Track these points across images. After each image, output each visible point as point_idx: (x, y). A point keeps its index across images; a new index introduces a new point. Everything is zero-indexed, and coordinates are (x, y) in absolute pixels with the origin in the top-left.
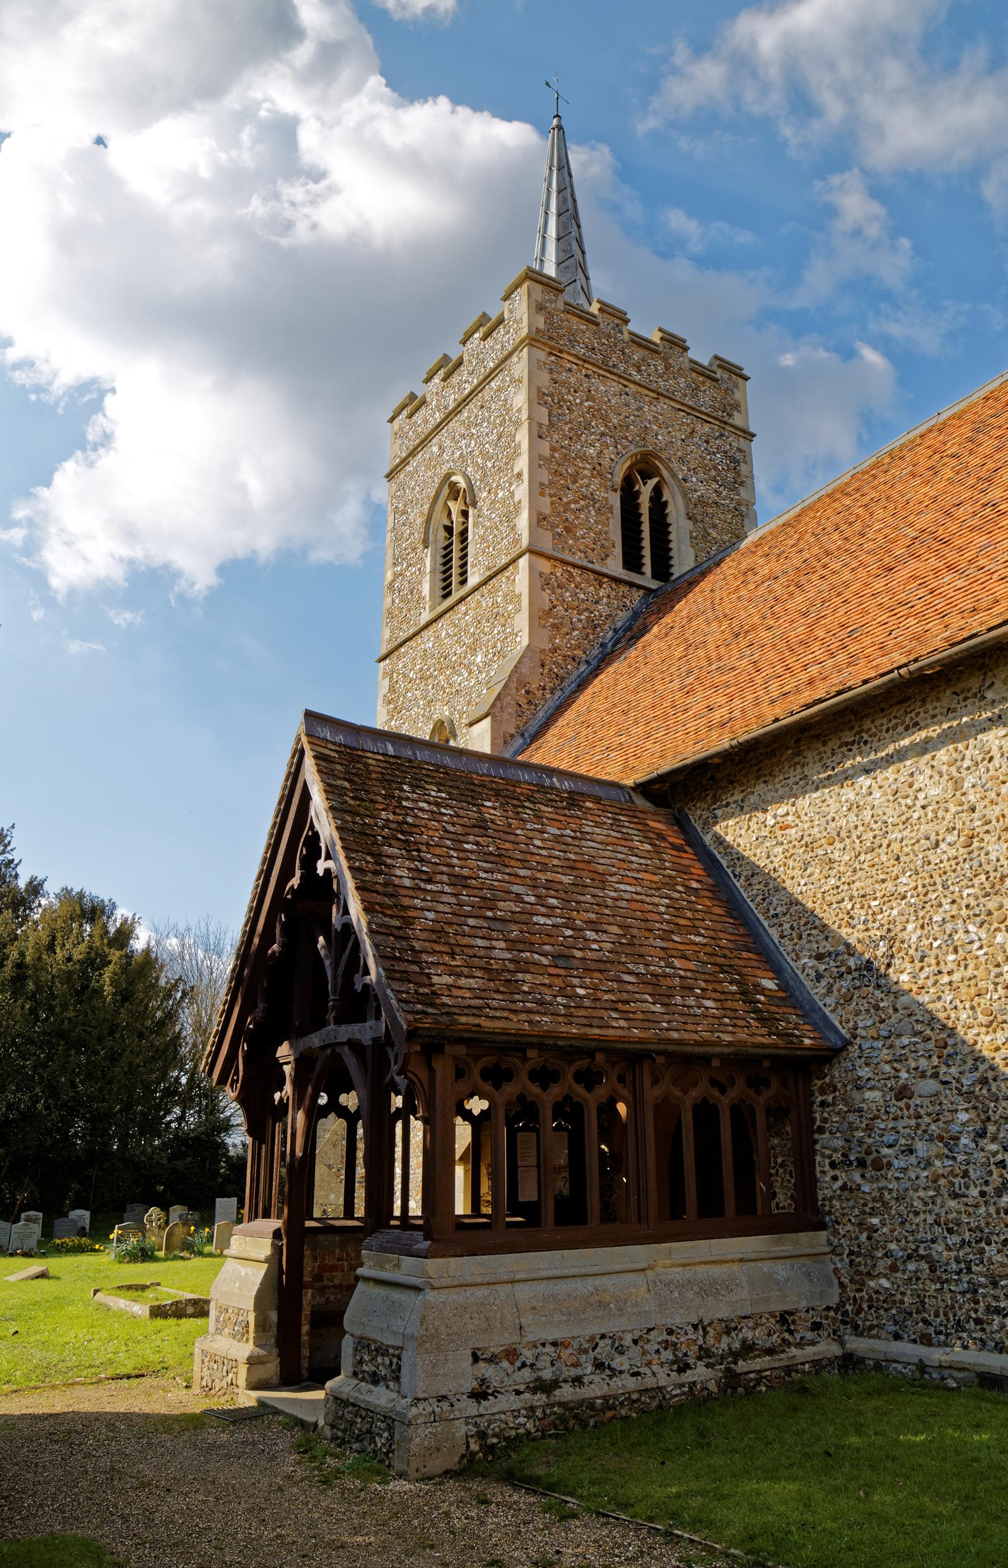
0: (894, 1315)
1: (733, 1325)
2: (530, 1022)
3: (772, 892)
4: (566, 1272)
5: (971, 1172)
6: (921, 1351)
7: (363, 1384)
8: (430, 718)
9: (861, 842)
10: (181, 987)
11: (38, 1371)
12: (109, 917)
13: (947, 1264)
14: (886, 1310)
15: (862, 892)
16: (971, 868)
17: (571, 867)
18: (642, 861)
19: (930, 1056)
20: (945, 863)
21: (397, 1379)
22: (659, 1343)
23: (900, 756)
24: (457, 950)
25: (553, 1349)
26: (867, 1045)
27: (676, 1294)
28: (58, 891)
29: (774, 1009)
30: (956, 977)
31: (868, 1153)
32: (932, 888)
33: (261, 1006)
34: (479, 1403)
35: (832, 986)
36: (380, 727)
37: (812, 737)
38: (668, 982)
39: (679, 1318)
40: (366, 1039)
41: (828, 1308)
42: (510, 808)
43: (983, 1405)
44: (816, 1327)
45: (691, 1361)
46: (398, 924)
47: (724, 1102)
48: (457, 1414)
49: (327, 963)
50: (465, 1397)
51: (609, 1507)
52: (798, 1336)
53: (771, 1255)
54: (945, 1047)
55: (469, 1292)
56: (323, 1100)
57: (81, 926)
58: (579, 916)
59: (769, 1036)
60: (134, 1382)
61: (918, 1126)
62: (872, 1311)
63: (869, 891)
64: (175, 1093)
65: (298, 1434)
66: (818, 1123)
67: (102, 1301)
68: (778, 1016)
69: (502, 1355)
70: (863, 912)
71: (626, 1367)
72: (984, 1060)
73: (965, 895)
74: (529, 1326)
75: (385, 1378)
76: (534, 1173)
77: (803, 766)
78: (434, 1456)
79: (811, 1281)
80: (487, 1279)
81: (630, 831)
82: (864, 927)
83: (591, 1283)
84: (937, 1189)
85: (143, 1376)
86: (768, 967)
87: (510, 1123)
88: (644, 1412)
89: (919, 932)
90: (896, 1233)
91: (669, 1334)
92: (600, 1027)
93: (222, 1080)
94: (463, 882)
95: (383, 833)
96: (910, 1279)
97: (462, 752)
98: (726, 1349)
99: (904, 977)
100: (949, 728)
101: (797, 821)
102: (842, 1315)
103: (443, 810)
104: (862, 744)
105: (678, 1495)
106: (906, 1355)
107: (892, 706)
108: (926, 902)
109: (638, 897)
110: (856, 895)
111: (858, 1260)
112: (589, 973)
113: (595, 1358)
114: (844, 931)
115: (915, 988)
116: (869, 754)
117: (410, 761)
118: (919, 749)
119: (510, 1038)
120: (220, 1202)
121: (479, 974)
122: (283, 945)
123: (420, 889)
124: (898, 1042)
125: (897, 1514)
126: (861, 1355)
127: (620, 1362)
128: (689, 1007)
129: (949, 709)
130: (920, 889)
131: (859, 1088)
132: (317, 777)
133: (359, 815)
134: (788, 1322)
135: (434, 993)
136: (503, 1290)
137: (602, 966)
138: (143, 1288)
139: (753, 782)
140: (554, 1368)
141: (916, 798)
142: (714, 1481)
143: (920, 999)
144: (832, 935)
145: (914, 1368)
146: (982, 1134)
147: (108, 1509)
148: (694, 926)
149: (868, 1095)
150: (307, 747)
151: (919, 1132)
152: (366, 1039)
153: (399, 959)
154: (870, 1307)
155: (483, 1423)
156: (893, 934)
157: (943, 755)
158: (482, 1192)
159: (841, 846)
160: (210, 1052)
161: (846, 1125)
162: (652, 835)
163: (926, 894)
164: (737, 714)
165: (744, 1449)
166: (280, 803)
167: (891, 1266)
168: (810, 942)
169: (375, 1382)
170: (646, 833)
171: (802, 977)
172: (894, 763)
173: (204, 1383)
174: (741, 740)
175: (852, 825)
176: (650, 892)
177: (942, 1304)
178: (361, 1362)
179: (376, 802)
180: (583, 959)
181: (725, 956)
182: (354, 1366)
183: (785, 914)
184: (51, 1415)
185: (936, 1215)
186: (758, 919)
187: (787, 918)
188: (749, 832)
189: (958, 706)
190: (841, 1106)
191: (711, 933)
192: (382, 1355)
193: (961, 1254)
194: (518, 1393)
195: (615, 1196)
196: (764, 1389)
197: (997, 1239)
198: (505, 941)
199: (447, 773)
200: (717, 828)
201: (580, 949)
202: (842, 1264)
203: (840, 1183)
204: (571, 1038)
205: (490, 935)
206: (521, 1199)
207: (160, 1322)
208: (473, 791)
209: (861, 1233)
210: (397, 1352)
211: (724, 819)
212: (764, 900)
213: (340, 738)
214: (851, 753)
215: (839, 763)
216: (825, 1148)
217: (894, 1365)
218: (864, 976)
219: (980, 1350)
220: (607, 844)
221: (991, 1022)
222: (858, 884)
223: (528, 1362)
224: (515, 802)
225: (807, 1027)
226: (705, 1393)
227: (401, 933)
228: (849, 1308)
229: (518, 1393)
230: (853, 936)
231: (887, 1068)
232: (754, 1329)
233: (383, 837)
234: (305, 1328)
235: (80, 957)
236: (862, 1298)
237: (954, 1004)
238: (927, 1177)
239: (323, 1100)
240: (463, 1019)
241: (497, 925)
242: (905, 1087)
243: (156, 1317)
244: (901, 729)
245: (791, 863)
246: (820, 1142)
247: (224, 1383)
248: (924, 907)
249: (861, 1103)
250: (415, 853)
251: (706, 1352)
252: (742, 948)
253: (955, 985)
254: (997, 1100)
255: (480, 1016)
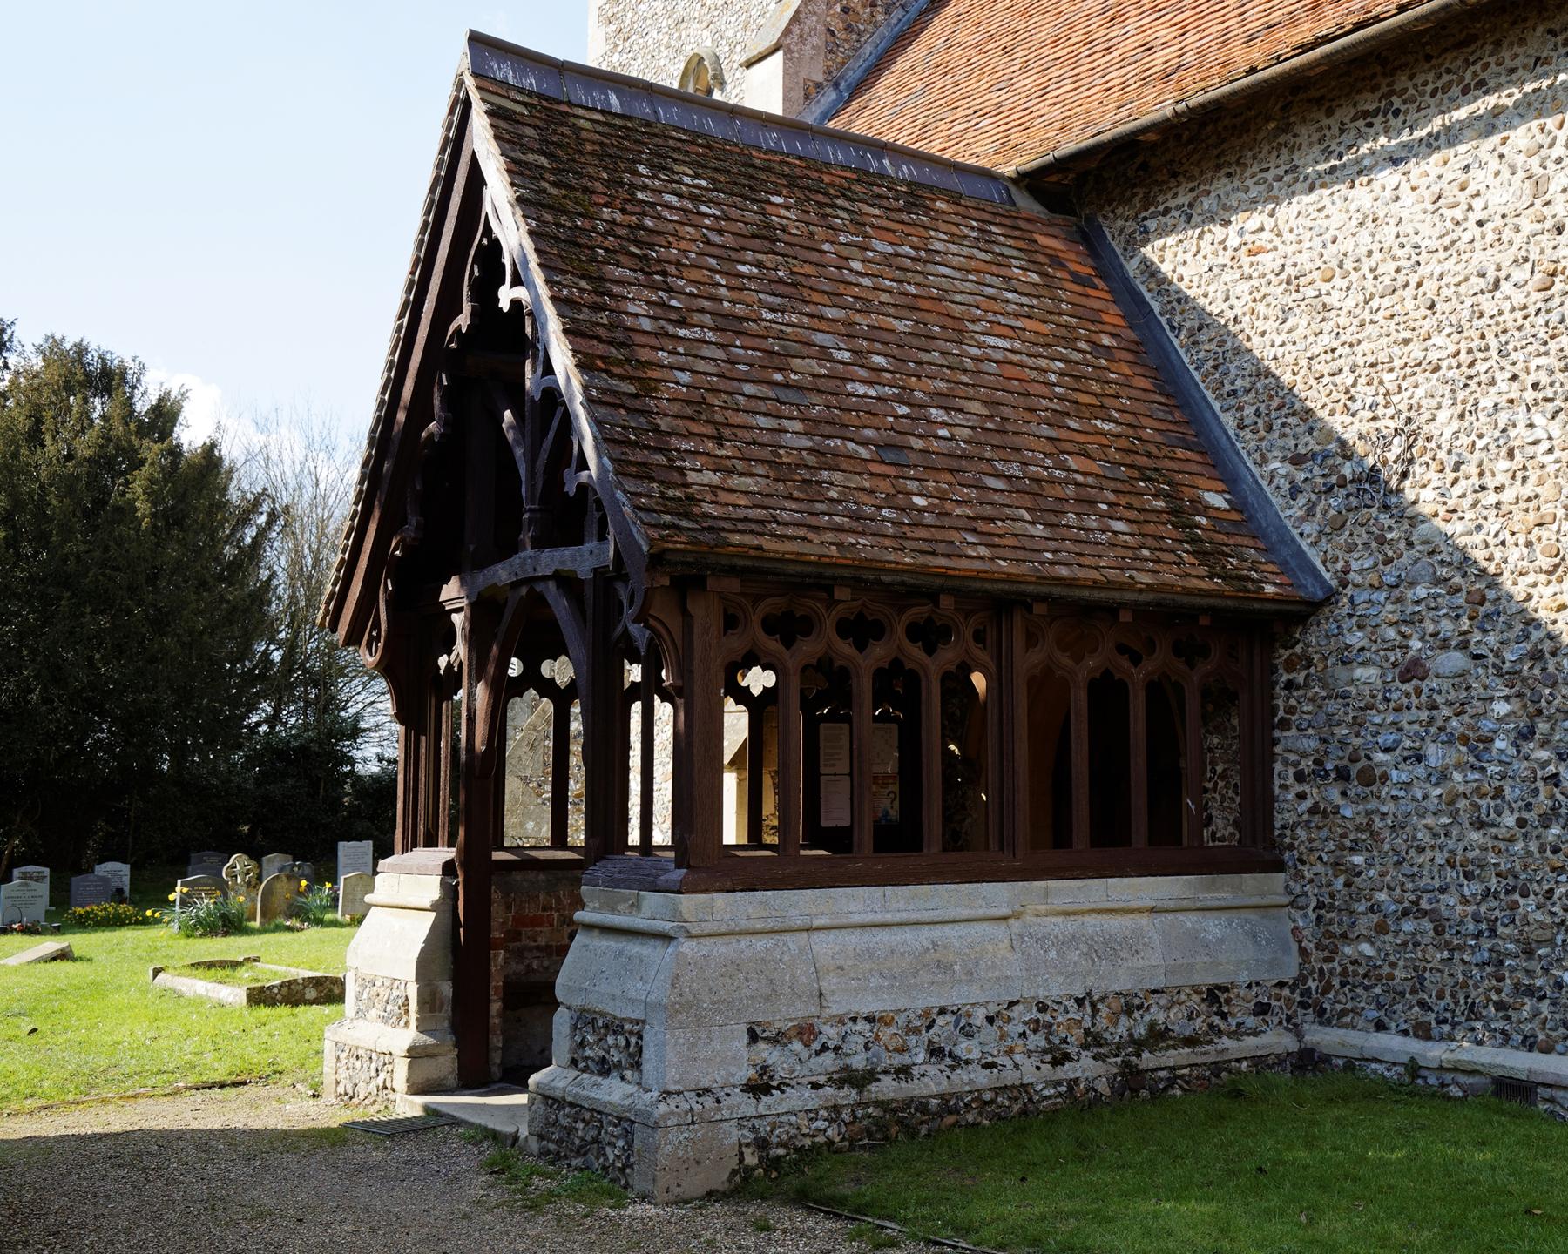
0: (1378, 996)
1: (1137, 1001)
2: (840, 545)
3: (1229, 355)
4: (889, 917)
5: (1507, 790)
6: (1414, 1046)
7: (585, 1076)
8: (679, 51)
9: (1376, 278)
10: (265, 508)
11: (80, 1079)
12: (134, 387)
13: (1461, 923)
14: (1366, 988)
15: (1371, 359)
16: (1547, 324)
17: (910, 307)
18: (1024, 300)
19: (1458, 616)
20: (1507, 316)
21: (637, 1065)
22: (1025, 1023)
23: (1451, 136)
24: (727, 432)
25: (868, 1026)
26: (1361, 597)
27: (1053, 954)
28: (39, 341)
29: (1221, 538)
30: (1507, 496)
31: (1354, 759)
32: (1482, 355)
33: (413, 521)
34: (759, 1099)
35: (1314, 505)
36: (595, 65)
37: (1309, 101)
38: (1057, 491)
39: (1054, 989)
40: (584, 570)
41: (1281, 985)
42: (812, 207)
43: (1495, 1118)
44: (1262, 1010)
45: (1072, 1050)
46: (632, 389)
47: (1138, 677)
48: (727, 1114)
49: (519, 452)
50: (737, 1090)
51: (944, 1233)
52: (1233, 1022)
53: (1199, 905)
54: (1482, 604)
55: (744, 942)
56: (515, 668)
57: (86, 401)
58: (921, 385)
59: (1211, 578)
60: (230, 1092)
61: (1432, 720)
62: (1346, 989)
63: (1383, 357)
64: (263, 677)
65: (489, 1150)
66: (1281, 713)
67: (169, 985)
68: (1227, 550)
69: (793, 1033)
70: (1371, 390)
71: (975, 1055)
72: (1539, 626)
73: (1533, 367)
74: (833, 993)
75: (618, 1066)
76: (845, 783)
77: (1292, 150)
78: (692, 1171)
79: (1257, 944)
80: (771, 924)
81: (1007, 251)
82: (1370, 415)
83: (926, 934)
84: (1454, 815)
85: (244, 1083)
86: (1216, 473)
87: (808, 706)
88: (1000, 1118)
89: (1456, 424)
90: (1388, 877)
91: (1040, 1010)
92: (948, 556)
93: (353, 639)
94: (736, 326)
95: (606, 244)
96: (1405, 944)
97: (735, 112)
98: (1125, 1035)
99: (1427, 494)
100: (1535, 91)
101: (1277, 241)
102: (1302, 995)
103: (703, 209)
104: (1390, 115)
105: (1042, 1218)
106: (1392, 1051)
107: (1446, 50)
108: (1470, 378)
109: (1016, 358)
110: (1361, 362)
111: (1329, 916)
112: (934, 475)
113: (930, 1041)
114: (1337, 422)
115: (1442, 511)
116: (1399, 134)
117: (648, 124)
118: (1481, 125)
119: (809, 569)
120: (344, 848)
121: (760, 470)
122: (445, 424)
123: (666, 334)
124: (1409, 594)
125: (1350, 1242)
126: (1325, 1051)
127: (966, 1048)
128: (1086, 530)
129: (1538, 59)
130: (1463, 356)
131: (1345, 662)
132: (494, 148)
133: (565, 212)
134: (1219, 1002)
135: (690, 498)
136: (794, 942)
137: (954, 464)
138: (235, 965)
139: (1209, 175)
140: (870, 1054)
141: (1470, 207)
142: (1096, 1200)
143: (1448, 528)
144: (1319, 425)
145: (1401, 1070)
146: (1527, 735)
147: (211, 1244)
148: (1102, 406)
149: (1360, 672)
150: (475, 96)
151: (1433, 730)
152: (584, 570)
153: (635, 444)
154: (1343, 985)
155: (764, 1127)
156: (1414, 427)
157: (1521, 136)
158: (765, 813)
159: (1345, 283)
160: (332, 594)
161: (1322, 718)
162: (1042, 259)
163: (1471, 365)
164: (1190, 58)
165: (1142, 1163)
166: (432, 191)
167: (1377, 925)
168: (1284, 435)
169: (605, 1073)
170: (1033, 256)
171: (1268, 490)
172: (1439, 148)
173: (341, 1090)
174: (1192, 103)
175: (1363, 250)
176: (1034, 350)
177: (1450, 981)
178: (582, 1045)
179: (593, 192)
180: (925, 451)
181: (1149, 455)
182: (573, 1051)
183: (1248, 391)
184: (106, 1135)
185: (1450, 852)
186: (1205, 398)
187: (1250, 398)
188: (1199, 257)
189: (1555, 54)
190: (1317, 689)
191: (1129, 418)
192: (615, 1033)
193: (1483, 909)
194: (815, 1086)
195: (969, 820)
196: (1178, 1093)
197: (1537, 888)
198: (802, 420)
199: (708, 147)
200: (1147, 251)
201: (920, 436)
202: (1305, 921)
203: (1308, 804)
204: (904, 571)
205: (779, 410)
206: (824, 823)
207: (264, 1012)
208: (752, 177)
209: (1336, 876)
210: (636, 1028)
211: (1160, 236)
212: (1215, 367)
213: (530, 82)
214: (1371, 131)
215: (1350, 147)
216: (1290, 751)
217: (1373, 1066)
218: (1365, 490)
219: (1501, 1045)
220: (968, 271)
221: (1556, 567)
222: (1365, 346)
223: (831, 1044)
224: (820, 198)
225: (1271, 568)
226: (1092, 1095)
227: (637, 404)
228: (1312, 984)
229: (815, 1086)
230: (1349, 428)
231: (1391, 633)
232: (1169, 1009)
233: (606, 250)
234: (495, 1007)
235: (88, 453)
236: (1332, 971)
237: (1501, 537)
238: (1440, 796)
239: (515, 668)
240: (736, 538)
241: (790, 395)
242: (1416, 662)
243: (258, 1003)
244: (1455, 91)
245: (1261, 308)
246: (1283, 742)
247: (372, 1087)
248: (1466, 385)
249: (1347, 684)
250: (657, 277)
251: (1095, 1039)
252: (1176, 442)
253: (1504, 509)
254: (1554, 685)
255: (762, 534)
